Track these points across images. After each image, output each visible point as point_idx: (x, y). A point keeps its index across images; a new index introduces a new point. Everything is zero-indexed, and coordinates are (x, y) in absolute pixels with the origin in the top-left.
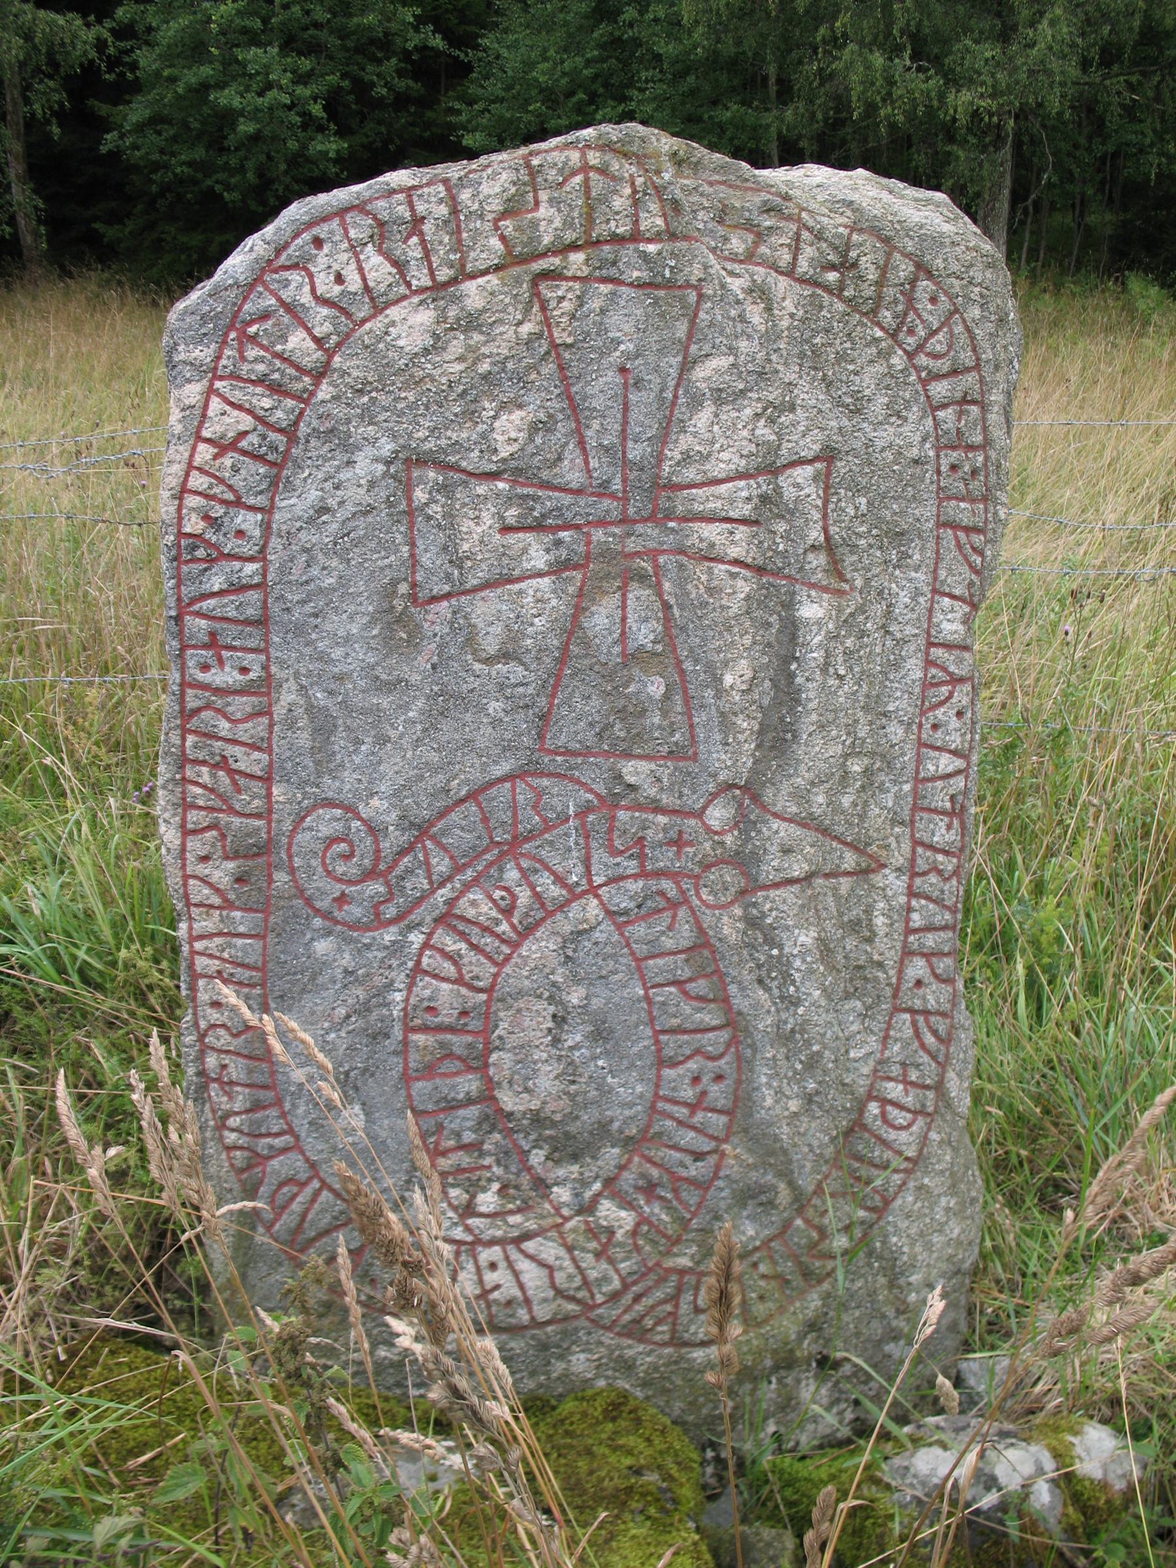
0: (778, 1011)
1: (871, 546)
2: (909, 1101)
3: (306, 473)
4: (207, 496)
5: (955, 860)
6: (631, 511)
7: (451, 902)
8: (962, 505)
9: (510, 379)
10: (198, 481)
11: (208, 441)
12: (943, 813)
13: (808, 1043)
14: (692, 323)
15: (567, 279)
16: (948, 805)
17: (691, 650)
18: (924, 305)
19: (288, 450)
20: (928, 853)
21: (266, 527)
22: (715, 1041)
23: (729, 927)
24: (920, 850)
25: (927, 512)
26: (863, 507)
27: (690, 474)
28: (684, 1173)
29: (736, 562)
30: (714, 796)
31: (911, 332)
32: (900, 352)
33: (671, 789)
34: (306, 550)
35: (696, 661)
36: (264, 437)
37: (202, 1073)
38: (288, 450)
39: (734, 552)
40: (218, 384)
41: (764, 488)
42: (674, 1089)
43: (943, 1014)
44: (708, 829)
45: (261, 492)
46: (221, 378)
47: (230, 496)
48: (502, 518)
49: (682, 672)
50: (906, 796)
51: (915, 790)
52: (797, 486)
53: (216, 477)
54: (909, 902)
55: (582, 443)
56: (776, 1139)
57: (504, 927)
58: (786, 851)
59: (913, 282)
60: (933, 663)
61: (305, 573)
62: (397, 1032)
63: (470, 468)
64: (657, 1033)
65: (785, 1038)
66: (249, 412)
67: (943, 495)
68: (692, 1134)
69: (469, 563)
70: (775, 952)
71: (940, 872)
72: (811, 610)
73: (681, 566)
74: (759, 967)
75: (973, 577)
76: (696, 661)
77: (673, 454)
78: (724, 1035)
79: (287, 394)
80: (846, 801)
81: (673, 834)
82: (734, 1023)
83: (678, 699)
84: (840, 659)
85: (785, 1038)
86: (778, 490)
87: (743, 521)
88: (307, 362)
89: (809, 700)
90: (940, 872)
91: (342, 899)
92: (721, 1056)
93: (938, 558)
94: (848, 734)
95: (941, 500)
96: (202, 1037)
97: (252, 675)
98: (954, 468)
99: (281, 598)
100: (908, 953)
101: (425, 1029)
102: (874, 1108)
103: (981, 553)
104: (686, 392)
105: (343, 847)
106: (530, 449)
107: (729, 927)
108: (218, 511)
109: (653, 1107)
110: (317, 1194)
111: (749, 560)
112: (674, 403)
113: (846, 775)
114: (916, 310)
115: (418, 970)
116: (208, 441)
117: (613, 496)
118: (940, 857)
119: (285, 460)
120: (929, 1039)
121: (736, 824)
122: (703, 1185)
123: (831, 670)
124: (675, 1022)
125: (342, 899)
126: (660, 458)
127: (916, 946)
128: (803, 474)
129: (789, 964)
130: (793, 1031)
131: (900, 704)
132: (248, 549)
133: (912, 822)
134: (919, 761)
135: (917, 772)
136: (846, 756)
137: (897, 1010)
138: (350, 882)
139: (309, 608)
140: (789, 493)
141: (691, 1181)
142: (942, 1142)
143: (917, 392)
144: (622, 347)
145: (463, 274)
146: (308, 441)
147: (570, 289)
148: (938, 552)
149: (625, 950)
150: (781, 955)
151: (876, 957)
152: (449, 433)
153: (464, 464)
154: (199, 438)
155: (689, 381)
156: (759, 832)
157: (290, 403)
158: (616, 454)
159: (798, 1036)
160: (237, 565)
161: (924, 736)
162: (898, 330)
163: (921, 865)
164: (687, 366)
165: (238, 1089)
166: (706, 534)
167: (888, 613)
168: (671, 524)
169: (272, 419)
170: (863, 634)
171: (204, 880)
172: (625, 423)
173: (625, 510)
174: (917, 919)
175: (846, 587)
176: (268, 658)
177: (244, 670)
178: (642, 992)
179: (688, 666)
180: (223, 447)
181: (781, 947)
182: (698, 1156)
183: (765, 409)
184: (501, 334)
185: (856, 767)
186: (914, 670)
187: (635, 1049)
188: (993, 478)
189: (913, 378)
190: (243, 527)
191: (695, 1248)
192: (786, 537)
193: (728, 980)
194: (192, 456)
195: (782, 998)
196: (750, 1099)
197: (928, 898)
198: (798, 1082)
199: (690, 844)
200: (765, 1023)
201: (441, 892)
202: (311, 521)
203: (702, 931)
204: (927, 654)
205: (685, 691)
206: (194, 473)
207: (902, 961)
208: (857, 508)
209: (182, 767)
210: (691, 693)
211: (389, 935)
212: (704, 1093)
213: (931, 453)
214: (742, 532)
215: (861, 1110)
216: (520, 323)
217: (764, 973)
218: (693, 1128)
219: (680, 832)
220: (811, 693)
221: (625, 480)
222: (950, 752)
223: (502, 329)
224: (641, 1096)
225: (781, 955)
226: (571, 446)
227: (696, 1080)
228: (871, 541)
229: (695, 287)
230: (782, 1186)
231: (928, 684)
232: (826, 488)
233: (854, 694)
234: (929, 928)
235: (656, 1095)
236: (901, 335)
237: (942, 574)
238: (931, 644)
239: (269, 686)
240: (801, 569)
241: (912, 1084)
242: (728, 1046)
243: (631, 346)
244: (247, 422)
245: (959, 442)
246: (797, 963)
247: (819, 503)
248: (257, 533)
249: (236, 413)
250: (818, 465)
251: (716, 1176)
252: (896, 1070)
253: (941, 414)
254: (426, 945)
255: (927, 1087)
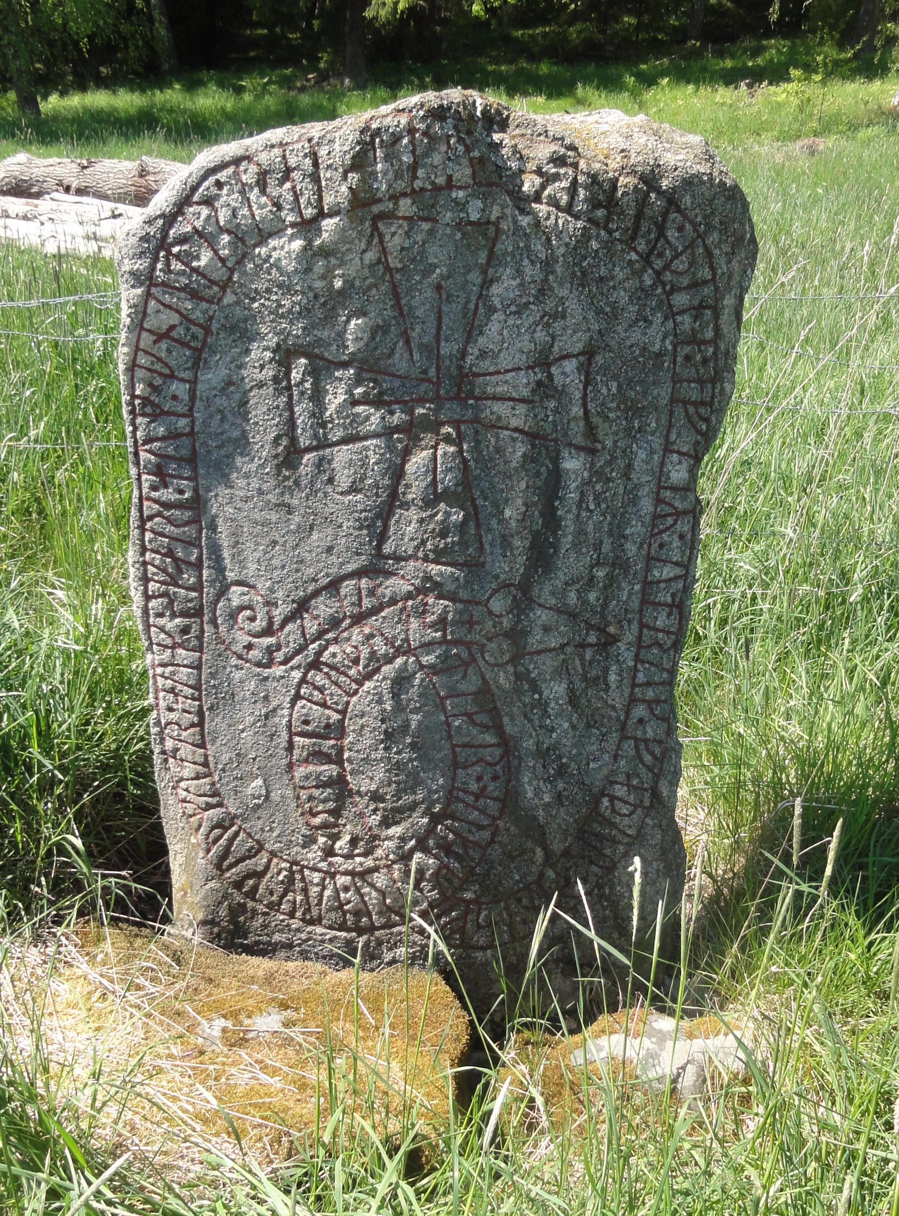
0: (537, 735)
1: (618, 417)
2: (631, 799)
3: (218, 357)
4: (149, 370)
5: (673, 637)
6: (442, 392)
7: (319, 653)
8: (692, 385)
9: (358, 294)
10: (142, 360)
11: (149, 331)
12: (666, 605)
13: (560, 757)
14: (491, 252)
15: (399, 218)
16: (669, 600)
17: (482, 492)
18: (672, 234)
19: (205, 339)
20: (652, 633)
21: (192, 393)
22: (488, 755)
23: (504, 679)
24: (645, 631)
25: (663, 393)
26: (614, 390)
27: (485, 365)
28: (471, 838)
29: (516, 430)
30: (495, 591)
31: (661, 255)
32: (650, 271)
33: (465, 587)
34: (221, 412)
35: (486, 499)
36: (188, 329)
37: (163, 752)
38: (205, 339)
39: (514, 423)
40: (153, 290)
41: (539, 376)
42: (465, 783)
43: (660, 742)
44: (490, 613)
45: (188, 369)
46: (156, 285)
47: (166, 371)
48: (352, 395)
49: (475, 507)
50: (637, 593)
51: (643, 590)
52: (564, 373)
53: (154, 356)
54: (636, 666)
55: (408, 342)
56: (535, 818)
57: (352, 672)
58: (546, 629)
59: (665, 214)
60: (663, 501)
61: (220, 427)
62: (285, 736)
63: (330, 358)
64: (453, 746)
65: (542, 754)
66: (177, 311)
67: (676, 380)
68: (476, 813)
69: (330, 426)
70: (536, 696)
71: (660, 646)
72: (572, 463)
73: (477, 432)
74: (525, 706)
75: (699, 437)
76: (486, 499)
77: (473, 350)
78: (498, 752)
79: (202, 299)
80: (592, 597)
81: (466, 617)
82: (507, 744)
83: (472, 524)
84: (591, 498)
85: (542, 754)
86: (550, 377)
87: (522, 401)
88: (215, 276)
89: (566, 526)
90: (660, 646)
91: (249, 647)
92: (497, 763)
93: (670, 426)
94: (595, 550)
95: (675, 383)
96: (161, 732)
97: (186, 496)
98: (687, 358)
99: (205, 444)
100: (633, 700)
101: (302, 734)
102: (605, 802)
103: (707, 420)
104: (484, 305)
105: (248, 613)
106: (373, 345)
107: (504, 679)
108: (158, 381)
109: (450, 792)
110: (236, 834)
111: (526, 429)
112: (475, 313)
113: (592, 578)
114: (666, 238)
115: (297, 697)
116: (149, 331)
117: (429, 381)
118: (660, 635)
119: (203, 347)
120: (648, 758)
121: (511, 611)
122: (483, 847)
123: (584, 505)
124: (466, 740)
125: (249, 647)
126: (463, 354)
127: (639, 695)
128: (570, 366)
129: (547, 704)
130: (548, 749)
131: (636, 528)
132: (180, 409)
133: (641, 611)
134: (648, 569)
135: (646, 577)
136: (592, 567)
137: (624, 738)
138: (255, 636)
139: (223, 452)
140: (558, 380)
141: (475, 843)
142: (654, 826)
143: (662, 301)
144: (438, 271)
145: (321, 215)
146: (218, 334)
147: (400, 226)
148: (670, 421)
149: (433, 691)
150: (541, 698)
151: (610, 702)
152: (315, 332)
153: (326, 354)
154: (142, 328)
155: (487, 296)
156: (527, 616)
157: (204, 305)
158: (431, 351)
159: (551, 752)
160: (173, 419)
161: (653, 552)
162: (649, 255)
163: (646, 640)
164: (487, 283)
165: (186, 764)
166: (495, 409)
167: (630, 466)
168: (471, 402)
169: (193, 317)
170: (609, 480)
171: (162, 629)
172: (439, 328)
173: (438, 392)
174: (641, 678)
175: (599, 447)
176: (197, 485)
177: (181, 492)
178: (444, 719)
179: (480, 502)
180: (160, 337)
181: (541, 694)
182: (481, 828)
183: (542, 318)
184: (351, 260)
185: (600, 573)
186: (647, 505)
187: (439, 756)
188: (721, 363)
189: (659, 290)
190: (176, 393)
191: (477, 887)
192: (556, 411)
193: (503, 713)
194: (138, 341)
195: (540, 727)
196: (517, 792)
197: (651, 664)
198: (551, 782)
199: (478, 623)
200: (529, 744)
201: (311, 646)
202: (223, 390)
203: (485, 681)
204: (658, 493)
205: (477, 519)
206: (140, 353)
207: (629, 704)
208: (609, 390)
209: (143, 554)
210: (481, 521)
211: (279, 671)
212: (485, 788)
213: (670, 348)
214: (521, 409)
215: (598, 802)
216: (364, 251)
217: (528, 709)
218: (477, 809)
219: (472, 616)
220: (569, 523)
221: (438, 369)
222: (672, 563)
223: (351, 256)
224: (442, 786)
225: (541, 698)
226: (401, 344)
227: (479, 779)
228: (619, 413)
229: (493, 223)
230: (538, 850)
231: (655, 517)
232: (587, 375)
233: (601, 522)
234: (648, 684)
235: (453, 785)
236: (653, 258)
237: (673, 437)
238: (660, 488)
239: (199, 503)
240: (566, 434)
241: (634, 786)
242: (502, 757)
243: (444, 270)
244: (175, 319)
245: (694, 340)
246: (553, 704)
247: (581, 386)
248: (187, 398)
249: (168, 311)
250: (581, 358)
251: (492, 841)
252: (621, 778)
253: (679, 319)
254: (303, 680)
255: (646, 790)
